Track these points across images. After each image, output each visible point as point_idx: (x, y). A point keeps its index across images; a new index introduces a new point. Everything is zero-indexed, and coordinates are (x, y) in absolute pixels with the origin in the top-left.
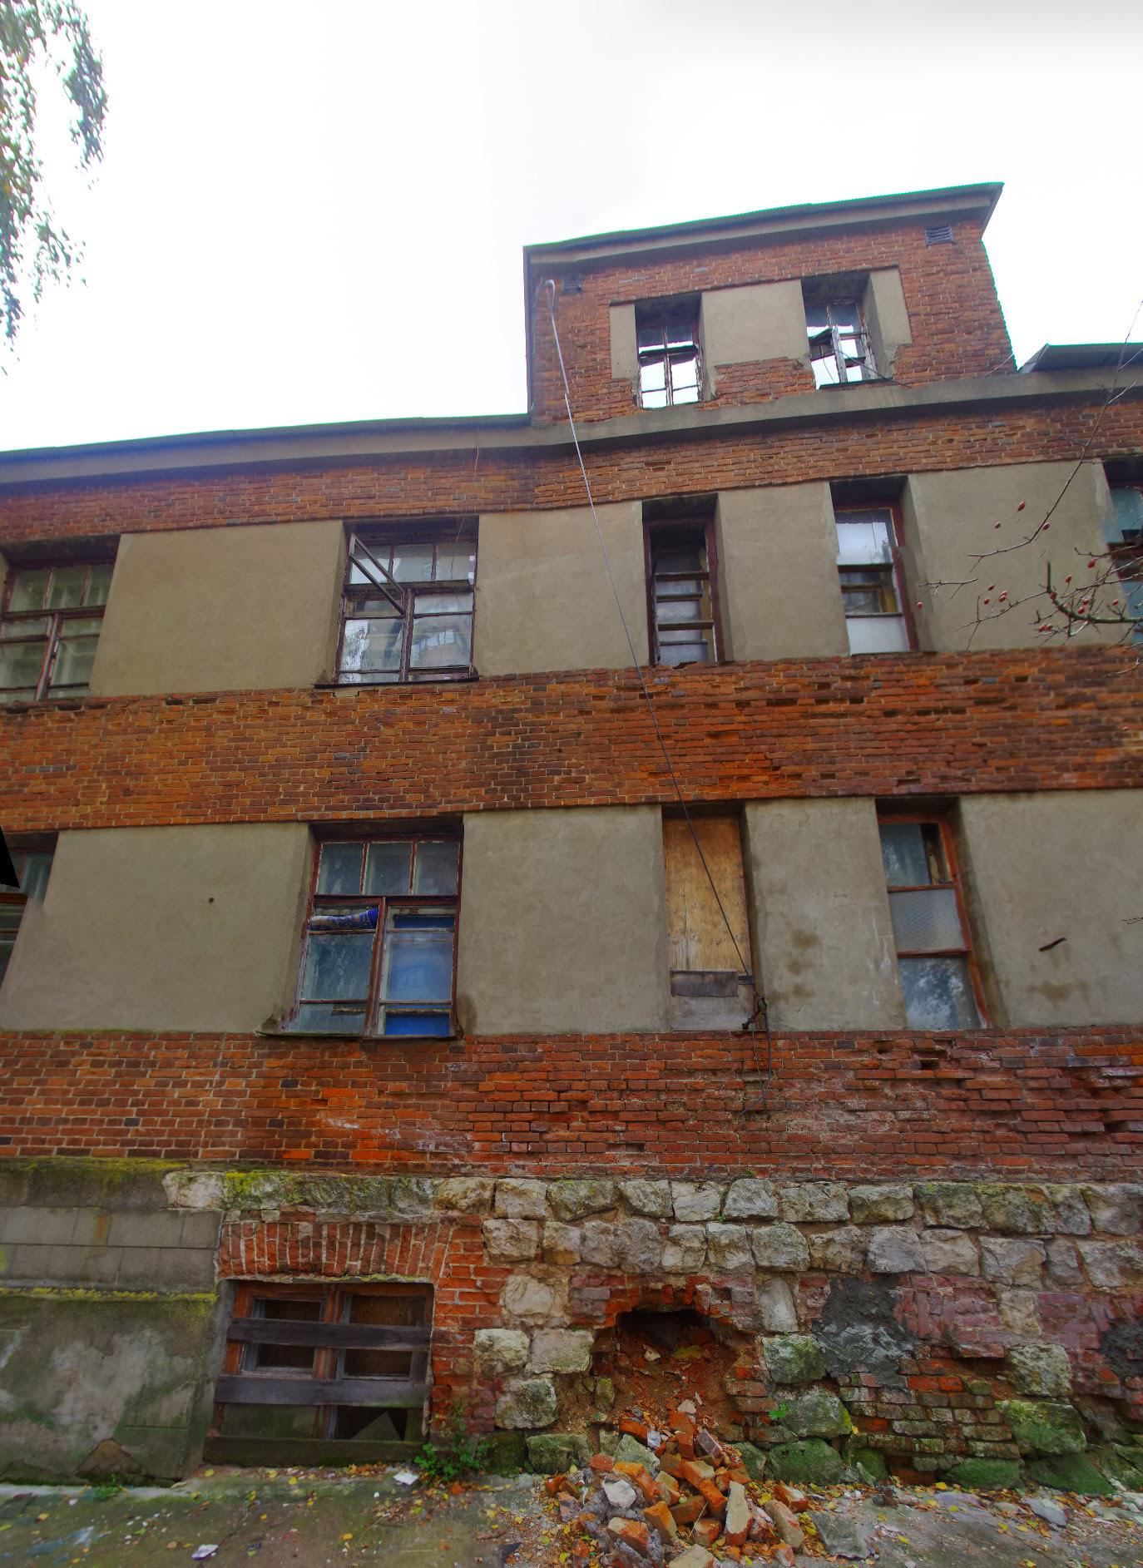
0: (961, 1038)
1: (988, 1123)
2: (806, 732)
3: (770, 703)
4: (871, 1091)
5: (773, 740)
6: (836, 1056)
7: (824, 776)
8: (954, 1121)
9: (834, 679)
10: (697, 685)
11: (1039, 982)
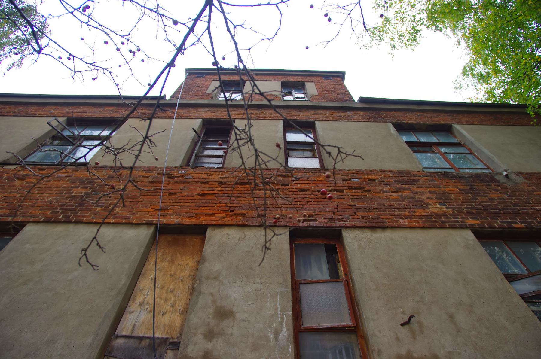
7: (259, 216)
10: (200, 175)
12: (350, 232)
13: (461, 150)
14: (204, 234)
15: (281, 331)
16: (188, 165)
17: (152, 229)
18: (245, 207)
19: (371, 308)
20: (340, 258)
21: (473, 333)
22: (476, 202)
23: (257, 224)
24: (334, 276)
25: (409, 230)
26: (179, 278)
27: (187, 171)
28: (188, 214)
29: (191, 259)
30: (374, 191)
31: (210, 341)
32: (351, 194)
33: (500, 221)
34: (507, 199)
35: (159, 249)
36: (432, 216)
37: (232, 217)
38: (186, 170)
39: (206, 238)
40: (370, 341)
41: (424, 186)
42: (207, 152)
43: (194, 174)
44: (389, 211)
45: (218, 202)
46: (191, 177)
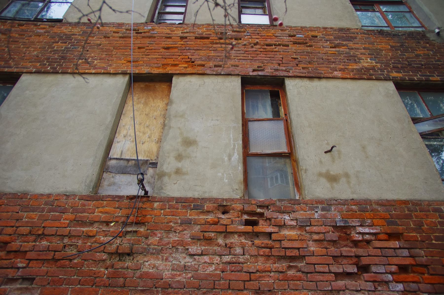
0: (274, 204)
1: (282, 265)
2: (211, 49)
3: (196, 38)
4: (209, 241)
5: (194, 51)
6: (192, 215)
7: (215, 66)
8: (260, 264)
9: (229, 31)
10: (164, 30)
11: (324, 171)
12: (291, 81)
13: (402, 8)
14: (171, 81)
15: (233, 155)
16: (152, 21)
17: (127, 78)
18: (204, 59)
19: (303, 140)
20: (281, 102)
21: (378, 159)
22: (403, 58)
23: (214, 73)
24: (276, 115)
25: (341, 81)
26: (153, 117)
27: (152, 27)
28: (156, 65)
29: (161, 102)
30: (315, 46)
31: (180, 161)
32: (295, 48)
33: (420, 75)
34: (432, 55)
35: (134, 94)
36: (362, 69)
37: (194, 67)
38: (151, 25)
39: (173, 85)
40: (300, 163)
41: (359, 43)
42: (169, 10)
43: (159, 30)
44: (326, 64)
45: (181, 54)
46: (156, 32)
